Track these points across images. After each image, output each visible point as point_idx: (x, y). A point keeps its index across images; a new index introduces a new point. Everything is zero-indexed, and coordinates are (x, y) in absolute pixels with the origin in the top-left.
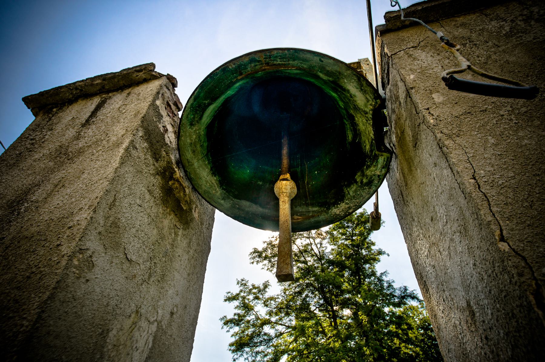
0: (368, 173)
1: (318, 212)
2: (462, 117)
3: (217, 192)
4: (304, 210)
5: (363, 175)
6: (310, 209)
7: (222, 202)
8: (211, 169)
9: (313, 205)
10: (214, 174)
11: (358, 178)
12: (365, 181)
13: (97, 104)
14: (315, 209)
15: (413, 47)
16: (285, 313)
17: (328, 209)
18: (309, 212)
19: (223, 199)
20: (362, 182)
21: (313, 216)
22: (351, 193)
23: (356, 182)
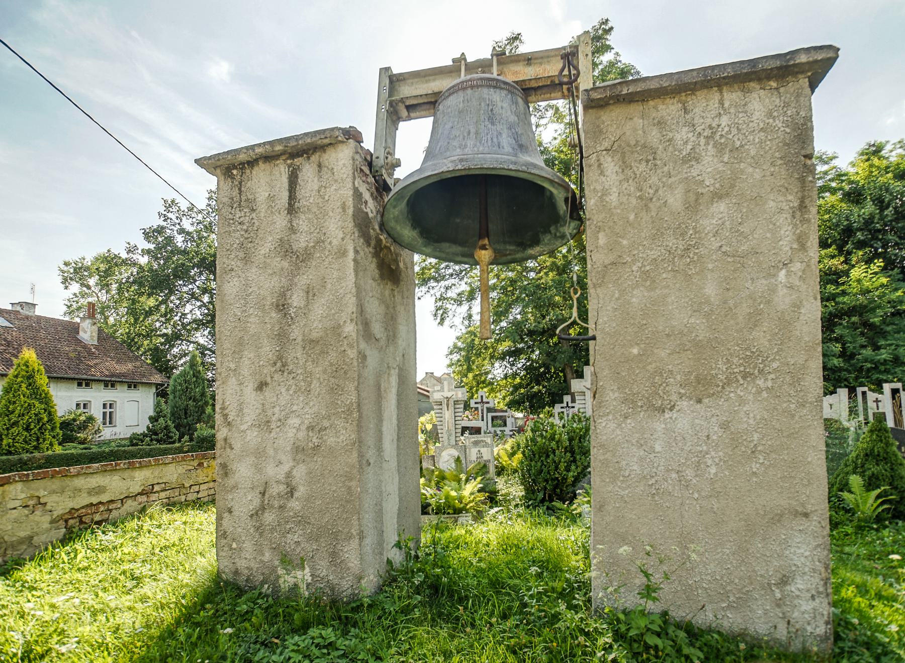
0: (561, 229)
1: (514, 251)
2: (609, 267)
3: (419, 242)
4: (502, 248)
5: (557, 229)
6: (508, 247)
7: (424, 249)
8: (412, 225)
9: (510, 243)
10: (414, 227)
11: (552, 229)
12: (558, 234)
13: (287, 176)
14: (512, 248)
15: (606, 150)
16: (519, 150)
17: (525, 249)
18: (507, 250)
19: (425, 246)
20: (555, 235)
21: (510, 254)
22: (546, 241)
23: (550, 232)
